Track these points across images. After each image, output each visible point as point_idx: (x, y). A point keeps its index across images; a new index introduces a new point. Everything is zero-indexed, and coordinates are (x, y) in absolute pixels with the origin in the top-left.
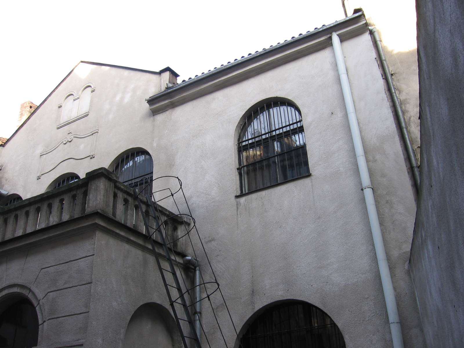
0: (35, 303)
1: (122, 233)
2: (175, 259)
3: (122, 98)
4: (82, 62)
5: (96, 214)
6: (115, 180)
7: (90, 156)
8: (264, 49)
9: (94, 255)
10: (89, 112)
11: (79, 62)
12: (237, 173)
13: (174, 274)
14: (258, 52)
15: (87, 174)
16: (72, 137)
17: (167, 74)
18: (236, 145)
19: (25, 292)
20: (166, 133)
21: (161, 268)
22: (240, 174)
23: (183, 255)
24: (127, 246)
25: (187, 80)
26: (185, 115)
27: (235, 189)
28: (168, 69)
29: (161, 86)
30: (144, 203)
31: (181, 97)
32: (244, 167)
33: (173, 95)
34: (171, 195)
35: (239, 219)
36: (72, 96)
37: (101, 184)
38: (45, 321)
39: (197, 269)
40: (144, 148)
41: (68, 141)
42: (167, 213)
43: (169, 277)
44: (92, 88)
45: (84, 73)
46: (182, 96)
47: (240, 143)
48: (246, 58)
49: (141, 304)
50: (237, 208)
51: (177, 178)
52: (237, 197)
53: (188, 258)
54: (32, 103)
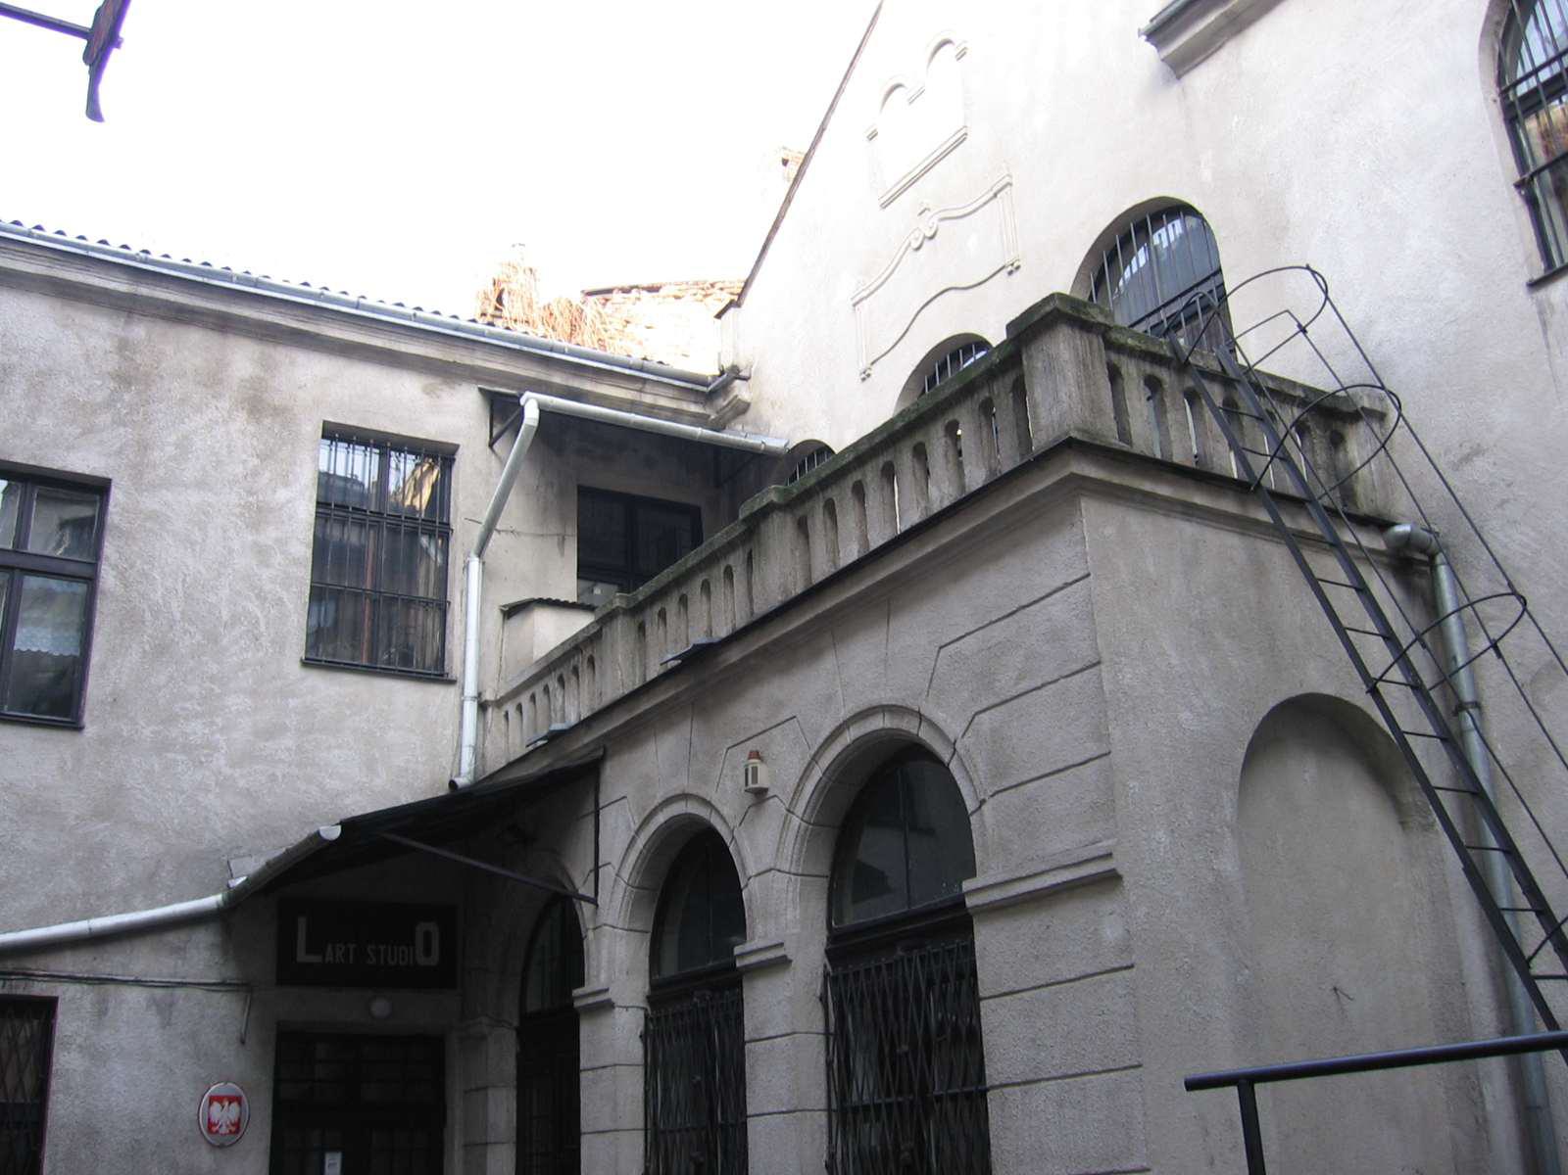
5: (1069, 446)
6: (1100, 324)
9: (1088, 575)
13: (1362, 590)
15: (1009, 327)
16: (935, 219)
18: (1495, 101)
19: (909, 725)
20: (1234, 125)
22: (1532, 202)
23: (1380, 524)
24: (1188, 529)
27: (1521, 260)
30: (1211, 376)
32: (1538, 172)
38: (983, 802)
42: (1300, 393)
43: (1346, 602)
50: (1544, 324)
51: (1308, 268)
52: (1535, 285)
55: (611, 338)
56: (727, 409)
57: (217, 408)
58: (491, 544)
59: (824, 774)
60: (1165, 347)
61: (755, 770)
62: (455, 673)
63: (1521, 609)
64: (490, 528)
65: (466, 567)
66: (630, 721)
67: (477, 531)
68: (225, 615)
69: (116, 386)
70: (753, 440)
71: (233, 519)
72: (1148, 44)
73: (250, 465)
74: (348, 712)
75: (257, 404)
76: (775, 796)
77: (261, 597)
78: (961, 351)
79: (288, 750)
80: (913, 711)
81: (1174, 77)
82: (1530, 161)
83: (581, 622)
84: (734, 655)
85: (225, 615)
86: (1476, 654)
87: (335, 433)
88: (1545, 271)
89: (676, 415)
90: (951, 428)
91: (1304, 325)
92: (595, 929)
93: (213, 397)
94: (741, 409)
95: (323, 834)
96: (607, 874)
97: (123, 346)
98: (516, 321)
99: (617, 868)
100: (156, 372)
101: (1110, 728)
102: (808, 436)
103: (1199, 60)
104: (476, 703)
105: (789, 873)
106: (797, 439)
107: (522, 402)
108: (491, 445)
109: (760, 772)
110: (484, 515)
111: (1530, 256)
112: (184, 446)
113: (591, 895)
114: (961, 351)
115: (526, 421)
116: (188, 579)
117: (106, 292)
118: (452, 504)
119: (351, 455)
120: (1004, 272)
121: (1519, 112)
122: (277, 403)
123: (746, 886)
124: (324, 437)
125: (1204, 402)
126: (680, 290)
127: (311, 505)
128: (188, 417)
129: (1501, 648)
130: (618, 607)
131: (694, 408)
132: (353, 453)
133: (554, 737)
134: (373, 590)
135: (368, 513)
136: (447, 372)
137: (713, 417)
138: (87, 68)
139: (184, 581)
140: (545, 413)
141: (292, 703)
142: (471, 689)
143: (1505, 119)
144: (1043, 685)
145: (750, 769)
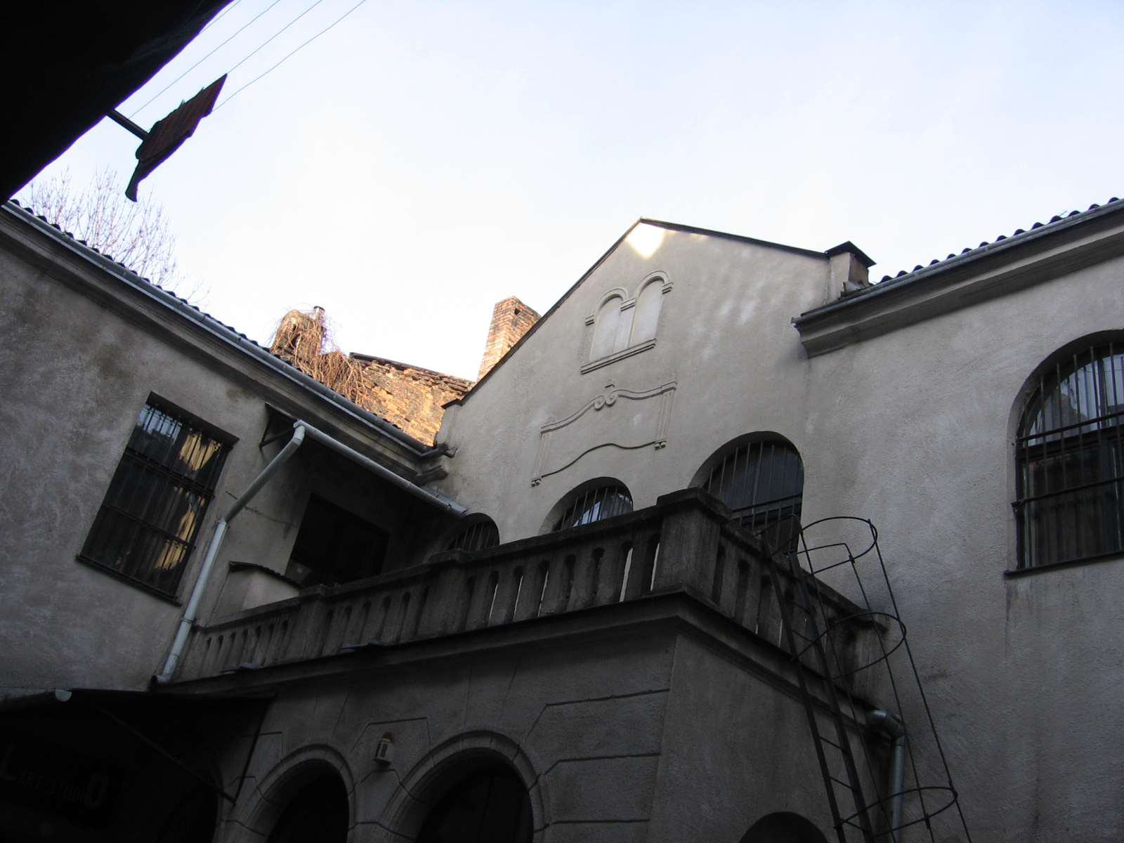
0: (528, 781)
1: (733, 645)
2: (852, 717)
3: (736, 312)
4: (643, 221)
5: (675, 597)
6: (722, 517)
7: (654, 443)
8: (1093, 207)
9: (668, 690)
10: (655, 339)
11: (635, 222)
12: (1012, 516)
13: (846, 752)
14: (1079, 214)
15: (660, 499)
16: (616, 395)
17: (845, 260)
18: (1013, 444)
19: (508, 752)
20: (837, 401)
21: (818, 735)
22: (1020, 519)
23: (865, 705)
24: (741, 676)
25: (893, 275)
26: (888, 362)
27: (1005, 555)
28: (848, 248)
29: (829, 288)
30: (783, 572)
31: (879, 318)
32: (1029, 501)
33: (857, 310)
34: (849, 559)
35: (1012, 631)
36: (618, 299)
37: (693, 524)
38: (547, 826)
39: (898, 741)
40: (782, 434)
41: (605, 403)
42: (836, 599)
43: (833, 755)
44: (666, 283)
45: (647, 243)
46: (880, 315)
47: (1023, 440)
48: (1047, 229)
49: (765, 812)
50: (1009, 602)
51: (869, 522)
52: (1009, 575)
53: (878, 713)
54: (520, 303)
55: (361, 392)
56: (430, 473)
57: (80, 358)
58: (239, 515)
59: (435, 767)
60: (758, 543)
61: (385, 747)
62: (183, 599)
63: (953, 799)
64: (242, 504)
65: (216, 527)
66: (300, 680)
67: (232, 504)
68: (34, 506)
69: (15, 319)
70: (444, 502)
71: (64, 440)
72: (796, 330)
73: (89, 405)
74: (97, 604)
75: (109, 365)
76: (394, 770)
77: (64, 502)
78: (607, 489)
79: (45, 617)
80: (514, 744)
81: (807, 357)
82: (1025, 491)
83: (285, 594)
84: (395, 660)
85: (34, 506)
86: (909, 822)
87: (156, 403)
88: (1018, 567)
89: (394, 466)
90: (598, 554)
91: (854, 556)
92: (228, 821)
93: (80, 350)
94: (441, 476)
95: (57, 695)
96: (250, 784)
97: (30, 294)
98: (300, 359)
99: (259, 782)
100: (47, 319)
101: (654, 802)
102: (482, 511)
103: (826, 351)
104: (190, 625)
105: (387, 829)
106: (474, 510)
107: (295, 425)
108: (261, 446)
109: (391, 749)
110: (242, 494)
111: (1011, 554)
112: (48, 377)
113: (233, 795)
114: (607, 489)
115: (292, 440)
116: (17, 472)
117: (32, 253)
118: (220, 478)
119: (161, 422)
120: (652, 447)
121: (1027, 457)
122: (123, 369)
123: (353, 828)
124: (148, 403)
125: (773, 587)
126: (418, 374)
127: (122, 447)
128: (58, 358)
129: (930, 822)
130: (318, 594)
131: (408, 465)
132: (164, 421)
133: (243, 672)
134: (138, 519)
135: (160, 466)
136: (246, 386)
137: (419, 475)
138: (136, 162)
139: (14, 472)
140: (308, 434)
141: (60, 584)
142: (190, 614)
143: (1016, 458)
144: (614, 757)
145: (382, 746)
